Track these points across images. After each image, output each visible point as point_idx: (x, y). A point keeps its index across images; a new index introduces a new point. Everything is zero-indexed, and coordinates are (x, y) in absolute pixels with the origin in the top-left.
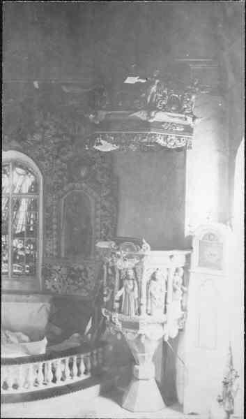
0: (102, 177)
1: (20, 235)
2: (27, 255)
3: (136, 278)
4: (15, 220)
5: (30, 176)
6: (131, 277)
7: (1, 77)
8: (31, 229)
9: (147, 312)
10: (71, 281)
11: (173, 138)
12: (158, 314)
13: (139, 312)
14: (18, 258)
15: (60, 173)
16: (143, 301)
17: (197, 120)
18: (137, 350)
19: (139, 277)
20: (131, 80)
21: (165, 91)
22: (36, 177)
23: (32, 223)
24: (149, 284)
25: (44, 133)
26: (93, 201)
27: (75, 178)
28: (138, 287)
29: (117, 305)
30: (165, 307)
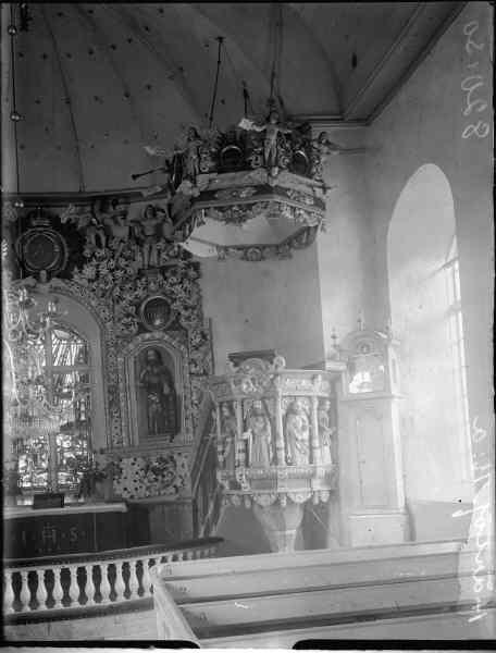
0: (188, 318)
3: (268, 415)
6: (259, 412)
8: (83, 418)
9: (286, 461)
11: (302, 212)
12: (301, 460)
13: (275, 460)
14: (65, 462)
15: (126, 320)
16: (281, 443)
17: (329, 191)
18: (274, 527)
19: (271, 412)
23: (83, 408)
24: (286, 419)
25: (97, 266)
28: (184, 603)
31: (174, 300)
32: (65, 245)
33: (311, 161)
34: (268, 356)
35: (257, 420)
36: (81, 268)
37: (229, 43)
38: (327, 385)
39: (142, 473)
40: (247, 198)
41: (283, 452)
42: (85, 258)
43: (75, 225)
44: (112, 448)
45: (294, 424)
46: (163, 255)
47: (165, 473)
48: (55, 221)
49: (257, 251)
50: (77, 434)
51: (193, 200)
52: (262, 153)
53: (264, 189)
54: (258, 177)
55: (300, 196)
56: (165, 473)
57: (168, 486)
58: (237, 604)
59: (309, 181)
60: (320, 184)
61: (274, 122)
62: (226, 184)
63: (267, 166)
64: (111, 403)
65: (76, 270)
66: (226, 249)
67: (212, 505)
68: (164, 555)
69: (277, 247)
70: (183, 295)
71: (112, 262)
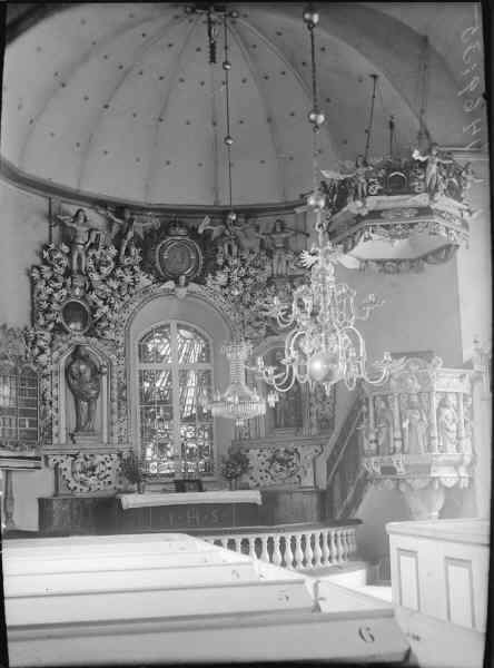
1: (189, 420)
2: (200, 447)
4: (183, 399)
5: (198, 341)
6: (415, 405)
7: (492, 382)
13: (429, 448)
16: (435, 433)
19: (425, 404)
22: (206, 341)
24: (439, 414)
29: (398, 444)
30: (217, 196)
32: (200, 254)
33: (461, 187)
34: (426, 356)
35: (414, 413)
36: (214, 274)
37: (382, 78)
38: (469, 385)
39: (268, 464)
40: (410, 218)
41: (436, 441)
42: (218, 265)
43: (210, 236)
44: (240, 439)
46: (292, 266)
47: (290, 464)
48: (193, 232)
49: (394, 265)
50: (198, 426)
51: (359, 218)
52: (424, 180)
53: (424, 211)
54: (422, 200)
55: (451, 217)
56: (290, 464)
57: (291, 475)
58: (224, 619)
59: (459, 205)
60: (466, 207)
61: (434, 153)
62: (391, 205)
63: (432, 191)
65: (210, 276)
66: (366, 261)
67: (352, 489)
68: (283, 535)
69: (412, 261)
71: (243, 270)
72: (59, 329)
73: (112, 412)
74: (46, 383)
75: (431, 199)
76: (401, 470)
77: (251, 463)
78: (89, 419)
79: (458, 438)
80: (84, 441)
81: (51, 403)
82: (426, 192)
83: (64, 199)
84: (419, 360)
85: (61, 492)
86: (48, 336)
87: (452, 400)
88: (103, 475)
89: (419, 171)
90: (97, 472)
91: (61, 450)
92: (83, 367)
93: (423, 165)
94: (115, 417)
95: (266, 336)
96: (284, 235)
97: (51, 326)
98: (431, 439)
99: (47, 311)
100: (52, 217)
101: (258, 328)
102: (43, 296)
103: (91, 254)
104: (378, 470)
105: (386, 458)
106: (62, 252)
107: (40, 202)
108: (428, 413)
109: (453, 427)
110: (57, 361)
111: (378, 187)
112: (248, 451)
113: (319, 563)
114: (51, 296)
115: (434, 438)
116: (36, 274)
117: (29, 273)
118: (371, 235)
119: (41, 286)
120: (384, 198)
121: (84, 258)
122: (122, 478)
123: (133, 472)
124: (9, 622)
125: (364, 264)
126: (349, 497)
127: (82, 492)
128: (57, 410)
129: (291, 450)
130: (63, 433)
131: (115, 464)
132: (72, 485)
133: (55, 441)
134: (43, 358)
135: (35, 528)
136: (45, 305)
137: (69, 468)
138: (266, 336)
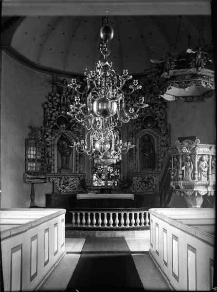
0: (161, 124)
10: (144, 185)
13: (194, 178)
20: (189, 51)
21: (205, 58)
24: (199, 163)
26: (155, 139)
27: (146, 127)
29: (181, 176)
31: (156, 117)
34: (193, 139)
40: (188, 79)
45: (202, 165)
46: (153, 99)
51: (167, 79)
52: (195, 62)
53: (195, 76)
57: (150, 188)
61: (200, 49)
62: (180, 74)
63: (197, 66)
64: (130, 155)
66: (178, 97)
69: (199, 96)
70: (160, 115)
72: (55, 127)
73: (77, 161)
74: (49, 149)
75: (197, 70)
76: (182, 187)
77: (134, 183)
78: (66, 163)
79: (208, 175)
80: (64, 172)
81: (51, 157)
82: (195, 67)
83: (58, 75)
84: (190, 140)
85: (55, 192)
86: (50, 130)
87: (205, 158)
88: (72, 186)
89: (192, 58)
90: (69, 184)
91: (55, 176)
92: (64, 143)
93: (195, 55)
94: (78, 163)
95: (141, 130)
96: (150, 86)
97: (51, 126)
98: (194, 174)
99: (51, 120)
100: (53, 83)
101: (138, 126)
102: (48, 114)
103: (69, 97)
104: (174, 187)
105: (176, 182)
106: (57, 97)
107: (49, 76)
108: (194, 163)
109: (206, 169)
110: (54, 140)
111: (175, 66)
112: (132, 178)
113: (143, 225)
114: (52, 114)
115: (196, 174)
116: (46, 106)
117: (43, 105)
118: (171, 87)
119: (47, 110)
120: (176, 70)
121: (65, 99)
122: (80, 187)
123: (85, 186)
124: (195, 290)
125: (177, 99)
126: (167, 198)
127: (63, 192)
128: (53, 160)
129: (150, 178)
130: (56, 169)
131: (77, 181)
132: (59, 189)
133: (52, 172)
134: (48, 139)
135: (44, 206)
136: (49, 118)
137: (58, 183)
138: (141, 130)
